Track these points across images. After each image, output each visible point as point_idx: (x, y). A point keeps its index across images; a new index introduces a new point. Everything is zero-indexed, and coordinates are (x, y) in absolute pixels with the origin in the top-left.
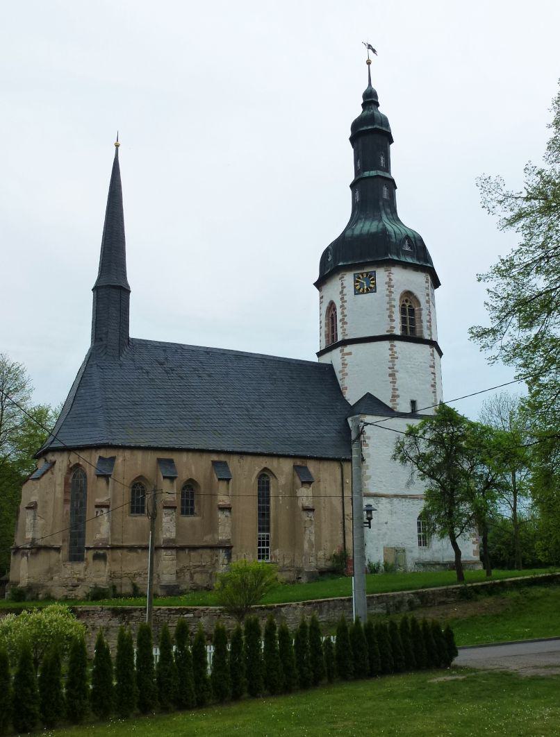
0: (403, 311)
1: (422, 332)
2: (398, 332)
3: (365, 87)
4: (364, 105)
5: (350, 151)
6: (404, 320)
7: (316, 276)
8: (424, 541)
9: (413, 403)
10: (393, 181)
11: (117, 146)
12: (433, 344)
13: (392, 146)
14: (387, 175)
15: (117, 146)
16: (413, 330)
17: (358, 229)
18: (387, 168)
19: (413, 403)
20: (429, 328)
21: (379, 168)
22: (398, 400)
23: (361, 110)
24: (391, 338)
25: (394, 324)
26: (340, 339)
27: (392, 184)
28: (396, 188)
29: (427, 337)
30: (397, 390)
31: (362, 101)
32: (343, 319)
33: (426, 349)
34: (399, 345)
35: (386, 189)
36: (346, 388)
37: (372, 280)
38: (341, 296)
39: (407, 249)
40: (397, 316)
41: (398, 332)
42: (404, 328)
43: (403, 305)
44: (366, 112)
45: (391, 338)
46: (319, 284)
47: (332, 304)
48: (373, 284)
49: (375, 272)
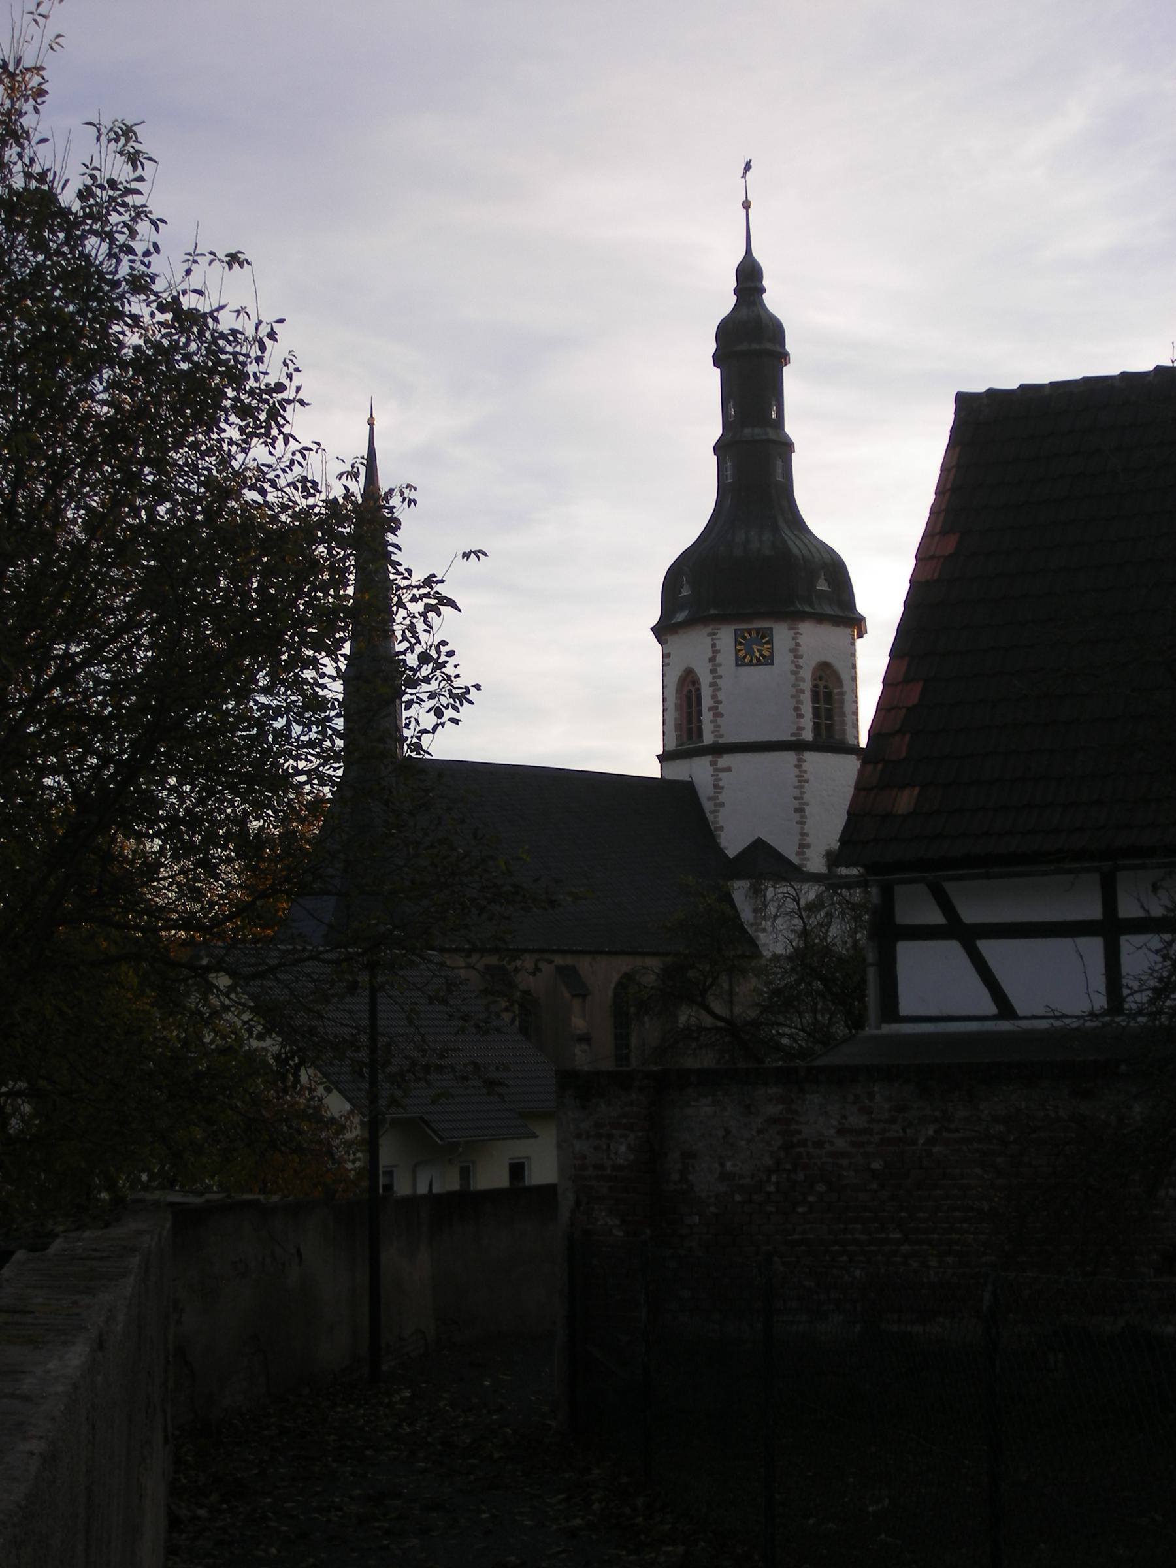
2: (808, 736)
34: (812, 759)
40: (807, 709)
41: (808, 736)
45: (797, 746)
49: (771, 629)
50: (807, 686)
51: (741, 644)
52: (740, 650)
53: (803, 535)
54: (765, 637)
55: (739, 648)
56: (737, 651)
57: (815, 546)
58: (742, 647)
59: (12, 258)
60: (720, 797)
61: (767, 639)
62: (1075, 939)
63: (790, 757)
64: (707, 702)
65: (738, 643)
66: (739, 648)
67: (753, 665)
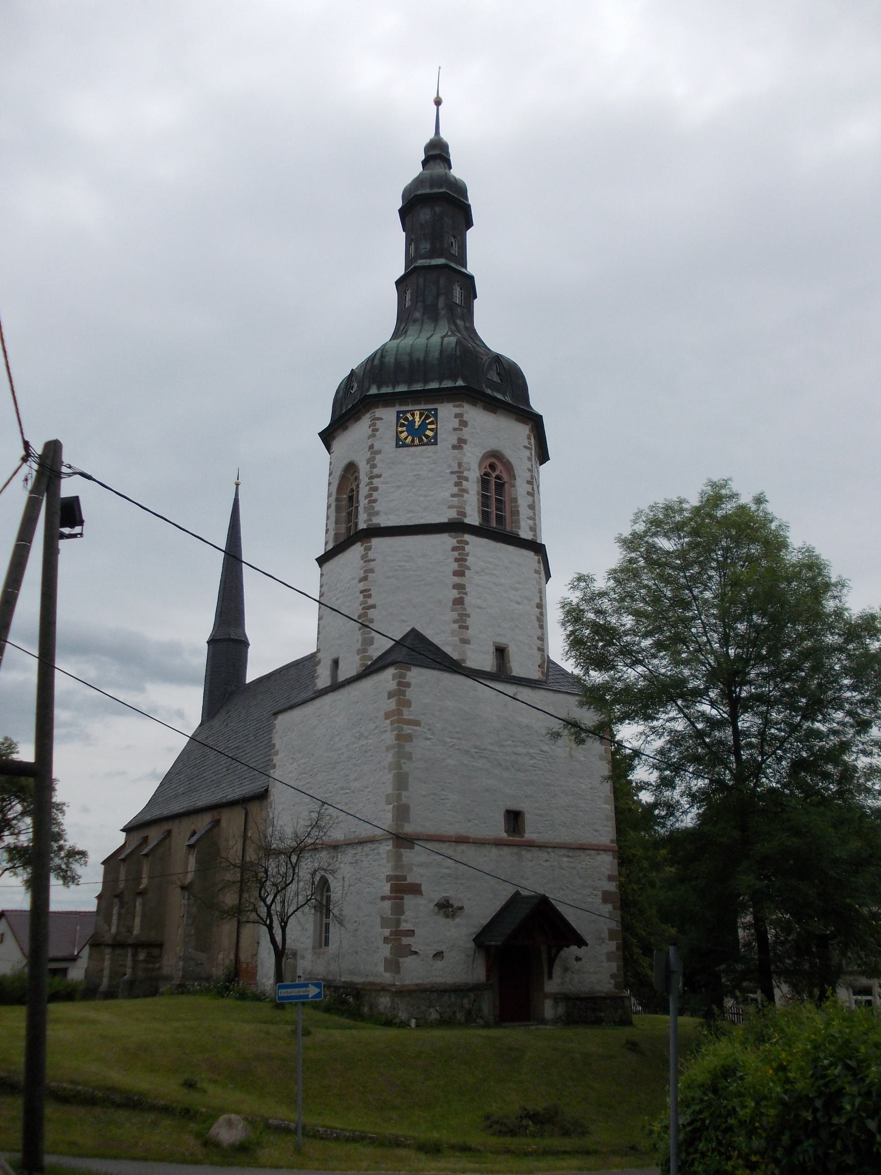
0: (484, 482)
1: (517, 522)
2: (473, 518)
3: (429, 135)
4: (425, 163)
5: (399, 237)
6: (485, 501)
7: (325, 421)
8: (557, 998)
9: (501, 652)
10: (471, 279)
11: (237, 485)
12: (538, 549)
13: (470, 234)
14: (464, 270)
15: (237, 485)
16: (500, 519)
17: (407, 341)
18: (462, 259)
19: (501, 652)
20: (534, 518)
21: (451, 257)
23: (420, 169)
24: (456, 527)
26: (362, 526)
27: (469, 284)
28: (475, 297)
29: (525, 534)
31: (400, 270)
32: (370, 495)
33: (530, 557)
34: (477, 546)
35: (458, 289)
36: (737, 491)
37: (431, 423)
38: (368, 455)
39: (496, 379)
40: (473, 488)
41: (473, 518)
42: (485, 515)
43: (486, 474)
44: (425, 172)
45: (456, 527)
46: (328, 437)
47: (351, 469)
48: (431, 430)
49: (436, 410)
50: (474, 474)
51: (402, 425)
52: (402, 432)
53: (484, 365)
54: (430, 418)
55: (400, 429)
56: (398, 433)
57: (532, 1025)
58: (404, 429)
59: (759, 1126)
60: (368, 613)
61: (431, 419)
62: (101, 884)
63: (447, 541)
64: (363, 502)
65: (399, 424)
66: (400, 429)
67: (416, 446)
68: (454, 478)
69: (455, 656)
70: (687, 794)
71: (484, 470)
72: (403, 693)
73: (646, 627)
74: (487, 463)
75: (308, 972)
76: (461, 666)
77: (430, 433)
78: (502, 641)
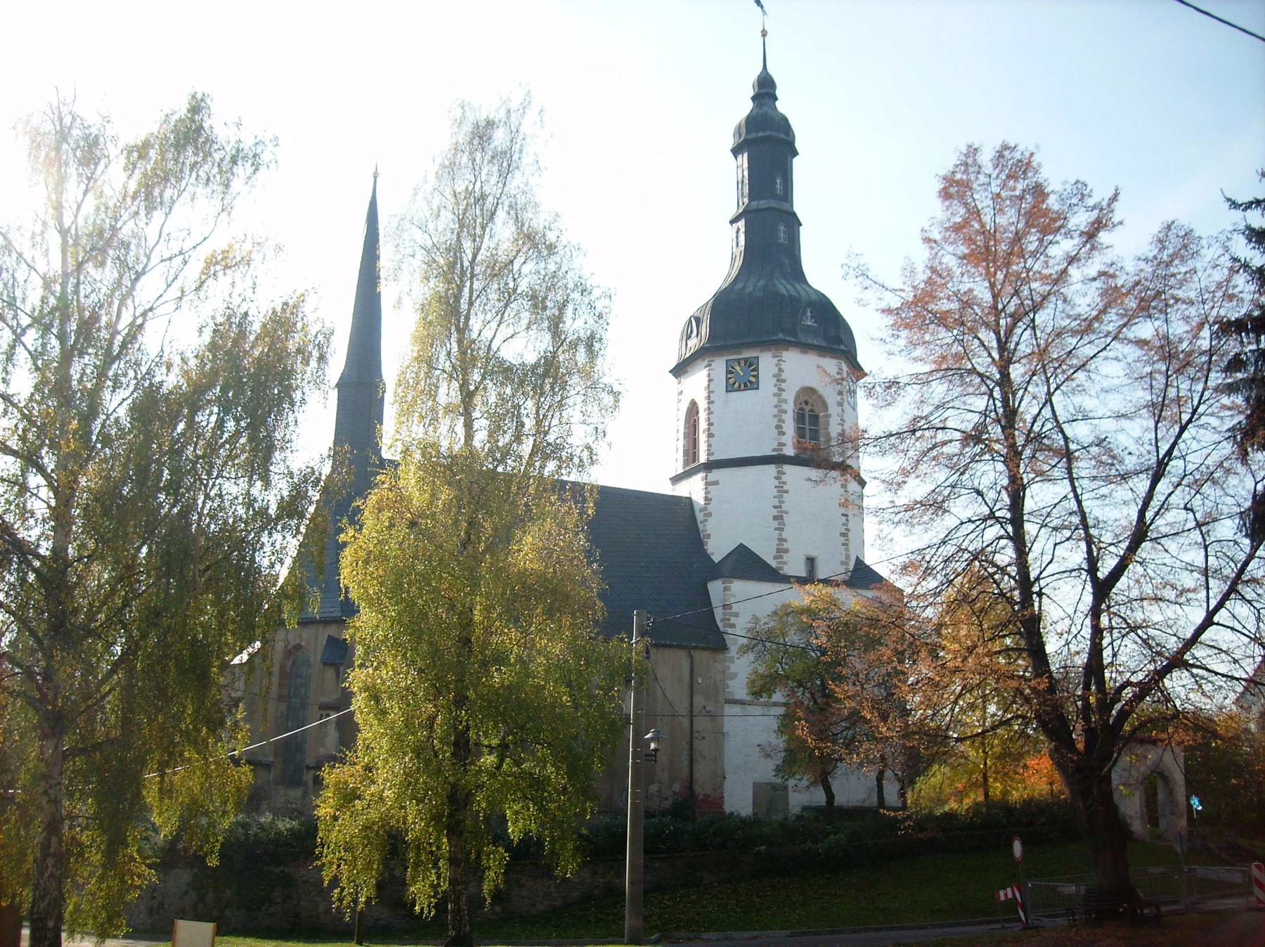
6: (800, 433)
9: (811, 561)
19: (811, 561)
22: (786, 557)
24: (778, 460)
25: (784, 439)
30: (786, 541)
34: (794, 474)
40: (790, 427)
45: (778, 460)
48: (754, 376)
50: (790, 407)
63: (771, 470)
68: (784, 376)
69: (773, 564)
70: (1208, 745)
71: (799, 406)
72: (780, 375)
73: (343, 889)
74: (802, 399)
75: (484, 124)
76: (779, 573)
77: (753, 379)
78: (812, 554)
